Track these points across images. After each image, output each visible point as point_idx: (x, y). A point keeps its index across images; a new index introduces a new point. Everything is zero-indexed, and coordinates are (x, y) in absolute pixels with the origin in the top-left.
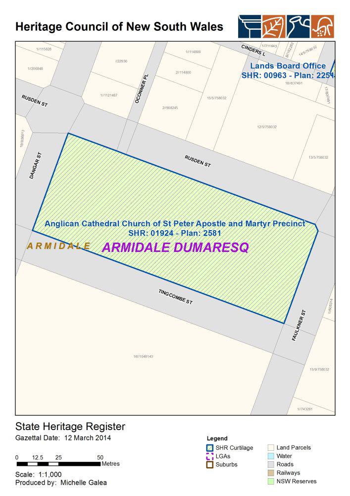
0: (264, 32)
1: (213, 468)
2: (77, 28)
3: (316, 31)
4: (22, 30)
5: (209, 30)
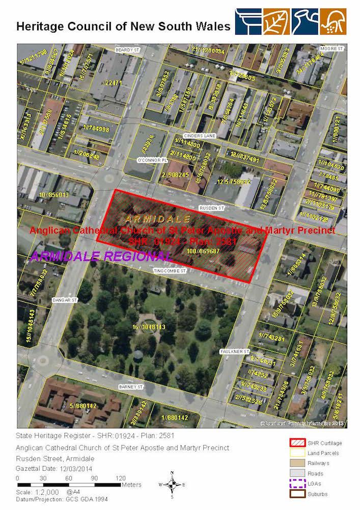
0: (265, 28)
1: (305, 497)
2: (80, 27)
3: (325, 27)
4: (23, 29)
5: (215, 29)
